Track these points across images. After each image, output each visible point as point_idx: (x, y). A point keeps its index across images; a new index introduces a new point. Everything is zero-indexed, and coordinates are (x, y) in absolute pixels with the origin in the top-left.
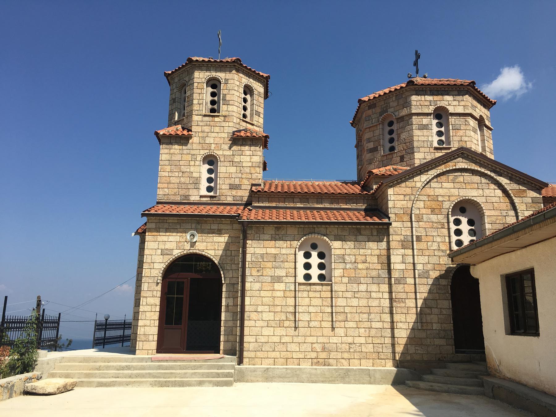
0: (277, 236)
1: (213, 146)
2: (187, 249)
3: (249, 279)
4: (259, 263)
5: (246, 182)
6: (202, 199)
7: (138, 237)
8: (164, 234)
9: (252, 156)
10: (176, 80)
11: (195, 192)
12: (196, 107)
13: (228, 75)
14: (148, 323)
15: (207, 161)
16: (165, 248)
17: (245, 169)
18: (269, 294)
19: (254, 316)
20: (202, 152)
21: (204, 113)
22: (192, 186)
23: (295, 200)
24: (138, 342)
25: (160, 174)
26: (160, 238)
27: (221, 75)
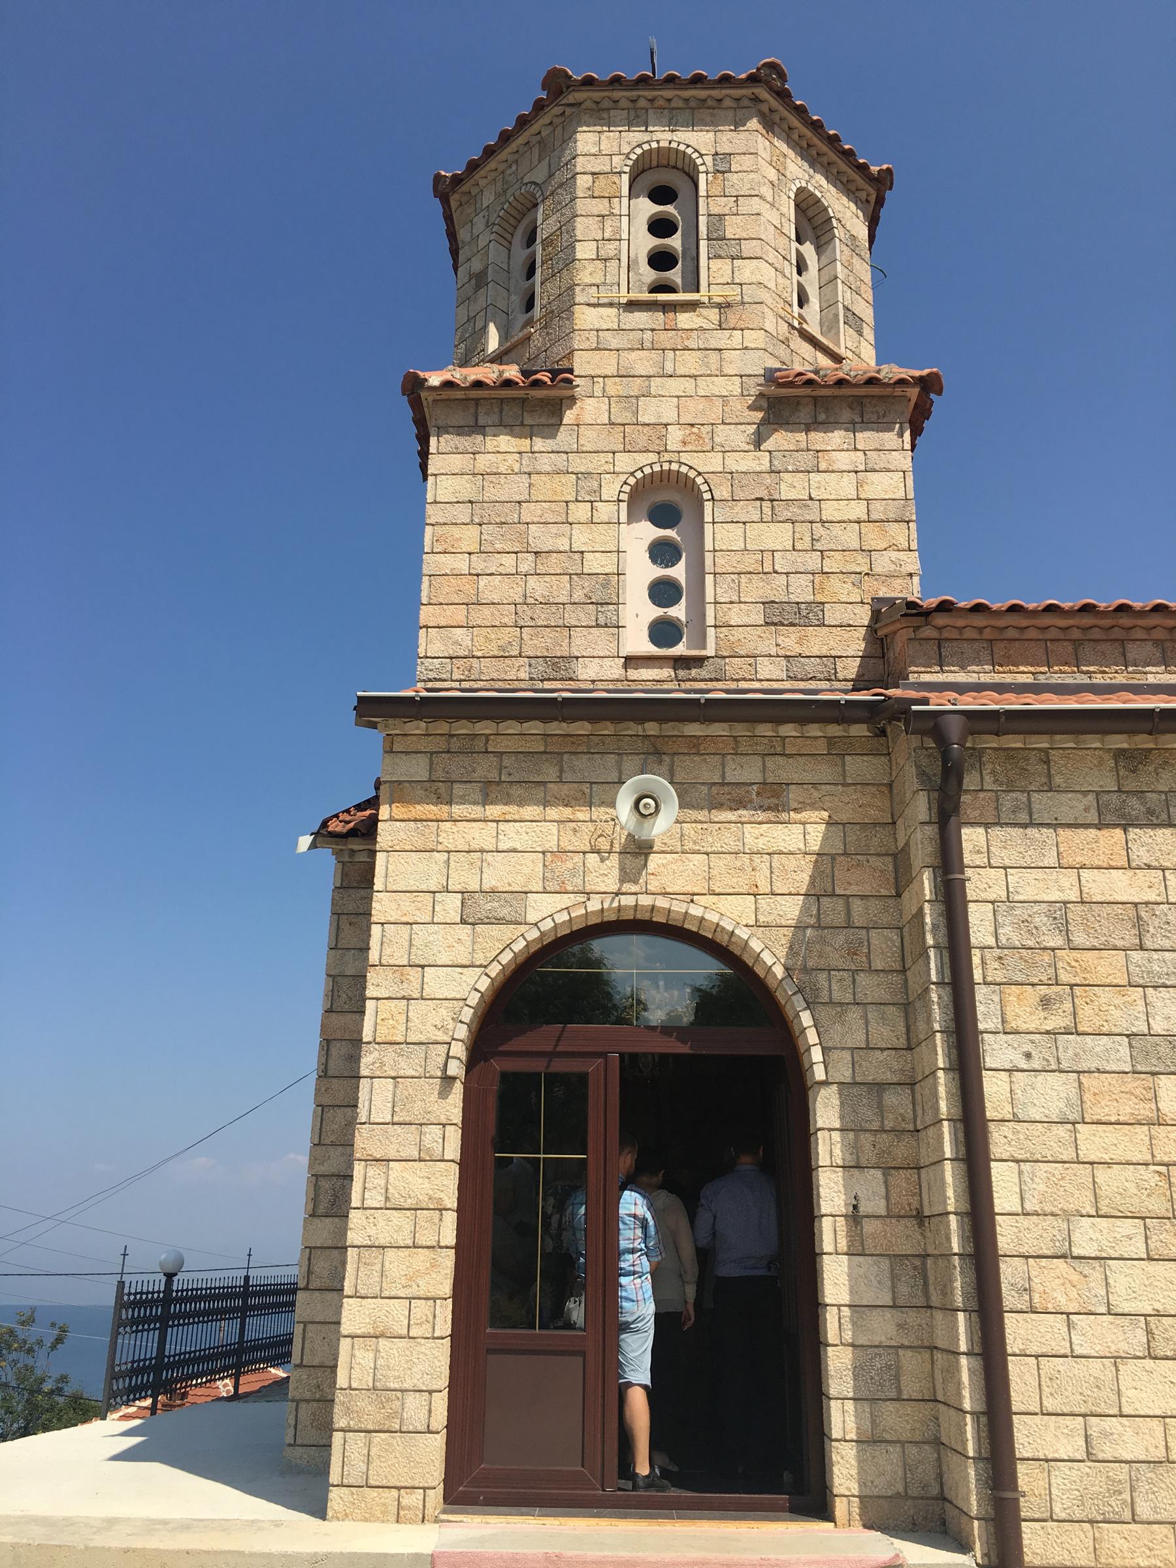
0: (1133, 802)
1: (675, 436)
2: (601, 888)
3: (996, 1052)
4: (1047, 957)
5: (843, 590)
6: (633, 674)
7: (327, 858)
8: (476, 811)
9: (864, 476)
10: (488, 198)
11: (600, 641)
12: (587, 274)
13: (729, 139)
14: (395, 1314)
15: (645, 507)
16: (470, 890)
17: (827, 545)
18: (1133, 1142)
19: (1055, 1283)
20: (625, 462)
21: (624, 297)
22: (585, 616)
23: (1133, 651)
24: (337, 1437)
25: (430, 564)
26: (452, 835)
27: (696, 141)
